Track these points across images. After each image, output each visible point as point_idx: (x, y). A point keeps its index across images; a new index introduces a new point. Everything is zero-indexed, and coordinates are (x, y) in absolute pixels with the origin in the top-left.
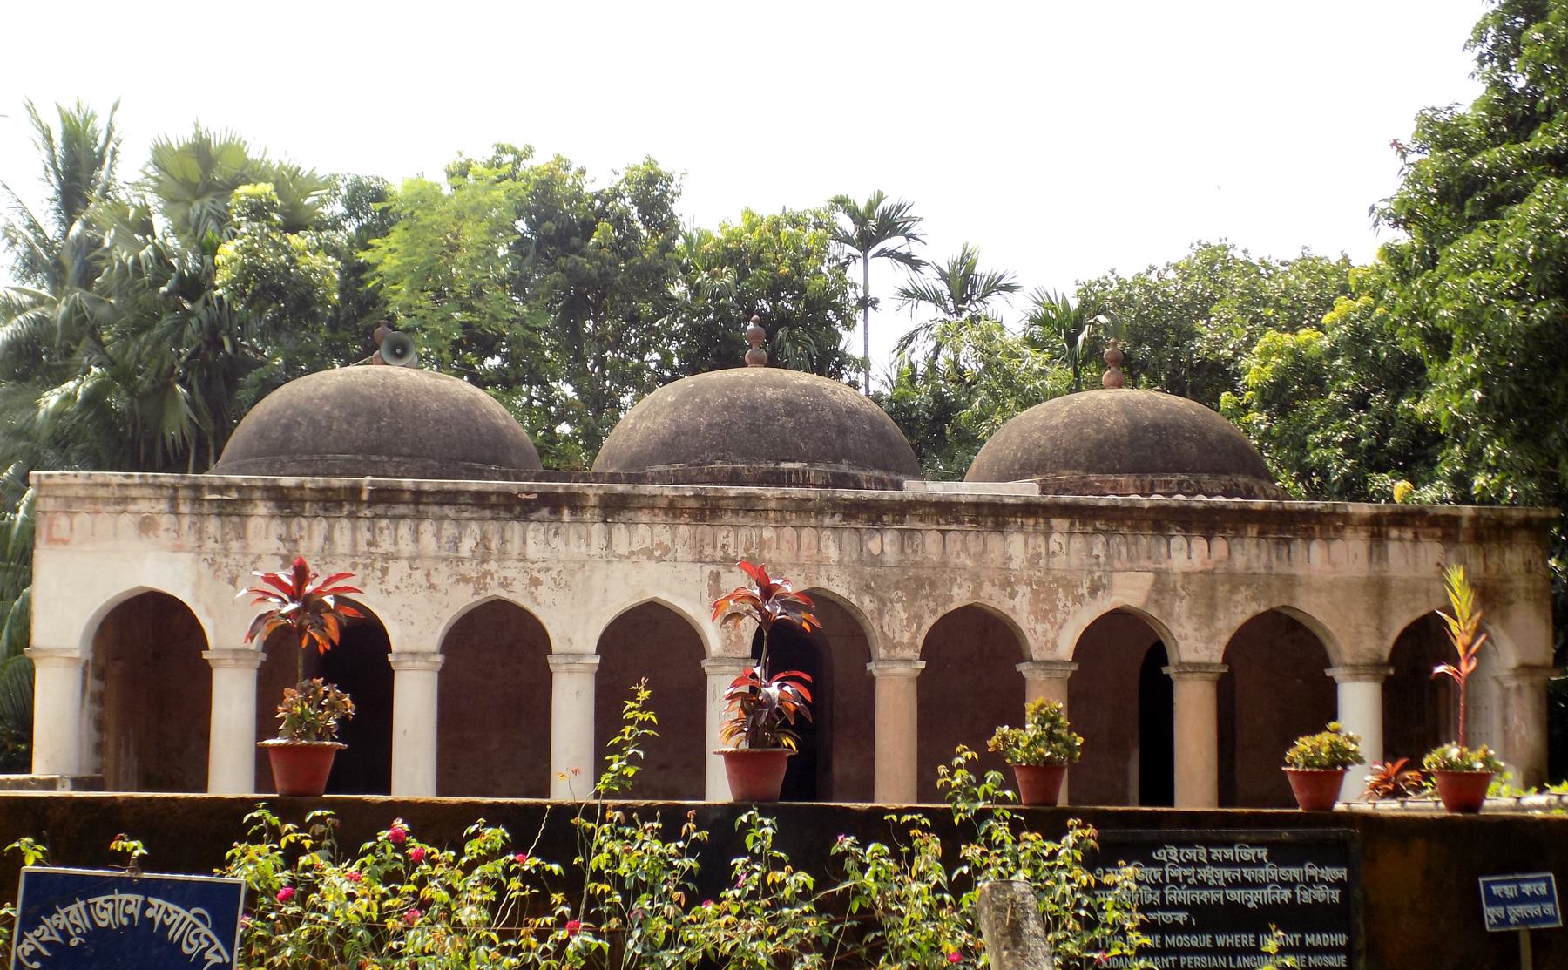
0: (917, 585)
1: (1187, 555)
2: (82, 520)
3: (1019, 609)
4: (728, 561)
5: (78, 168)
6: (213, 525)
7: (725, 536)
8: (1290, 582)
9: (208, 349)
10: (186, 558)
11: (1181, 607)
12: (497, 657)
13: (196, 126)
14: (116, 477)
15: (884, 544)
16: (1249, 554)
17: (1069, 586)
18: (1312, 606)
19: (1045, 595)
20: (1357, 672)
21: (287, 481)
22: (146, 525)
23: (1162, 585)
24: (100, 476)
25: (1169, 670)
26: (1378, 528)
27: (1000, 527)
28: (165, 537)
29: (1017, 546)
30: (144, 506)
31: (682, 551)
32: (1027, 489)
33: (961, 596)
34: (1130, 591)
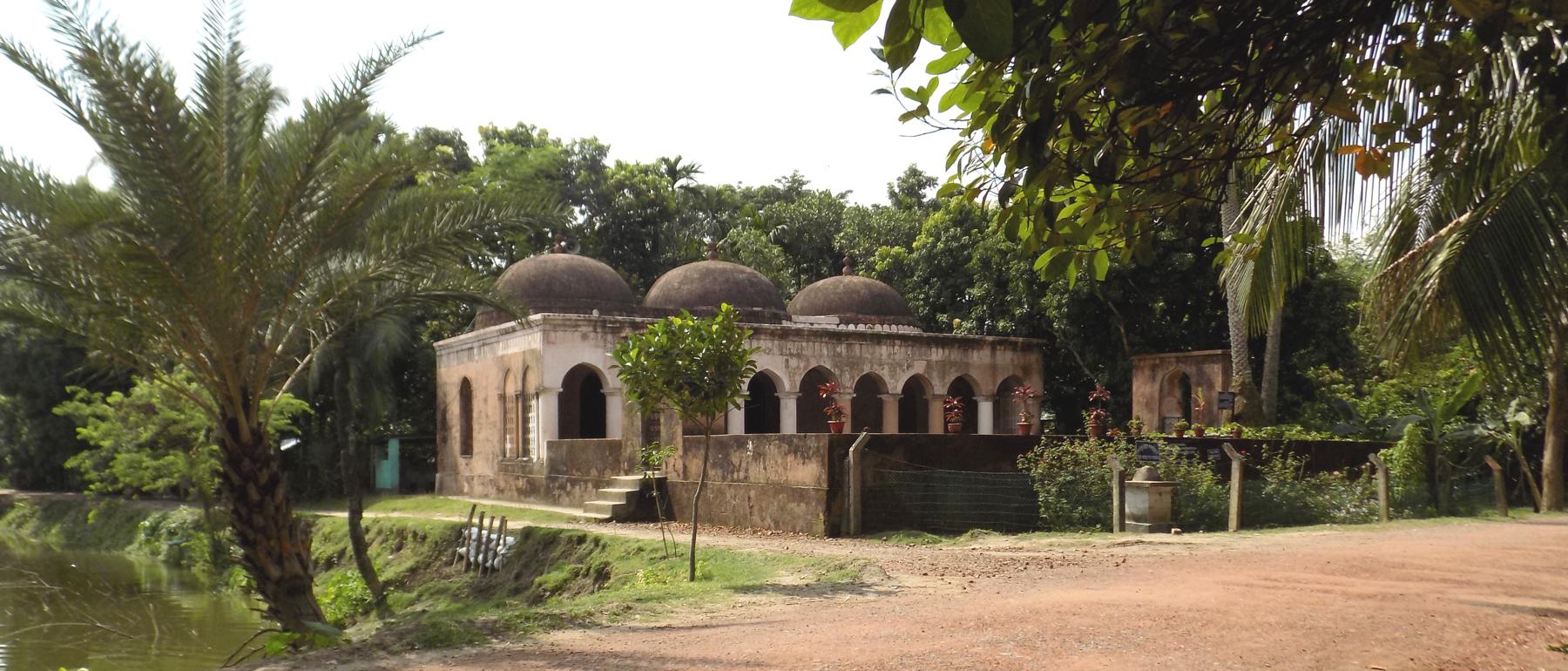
0: (854, 364)
1: (937, 355)
2: (560, 334)
3: (885, 374)
4: (791, 355)
5: (307, 103)
6: (609, 337)
7: (790, 345)
8: (967, 365)
9: (1241, 393)
10: (600, 351)
11: (935, 374)
12: (870, 387)
13: (210, 20)
14: (574, 316)
15: (842, 349)
16: (955, 355)
17: (901, 365)
18: (974, 374)
19: (895, 367)
20: (987, 398)
21: (639, 319)
22: (584, 337)
23: (929, 366)
24: (568, 316)
25: (929, 397)
26: (993, 345)
27: (879, 343)
28: (592, 342)
29: (884, 350)
30: (584, 329)
31: (776, 351)
32: (829, 322)
33: (867, 369)
34: (919, 368)
